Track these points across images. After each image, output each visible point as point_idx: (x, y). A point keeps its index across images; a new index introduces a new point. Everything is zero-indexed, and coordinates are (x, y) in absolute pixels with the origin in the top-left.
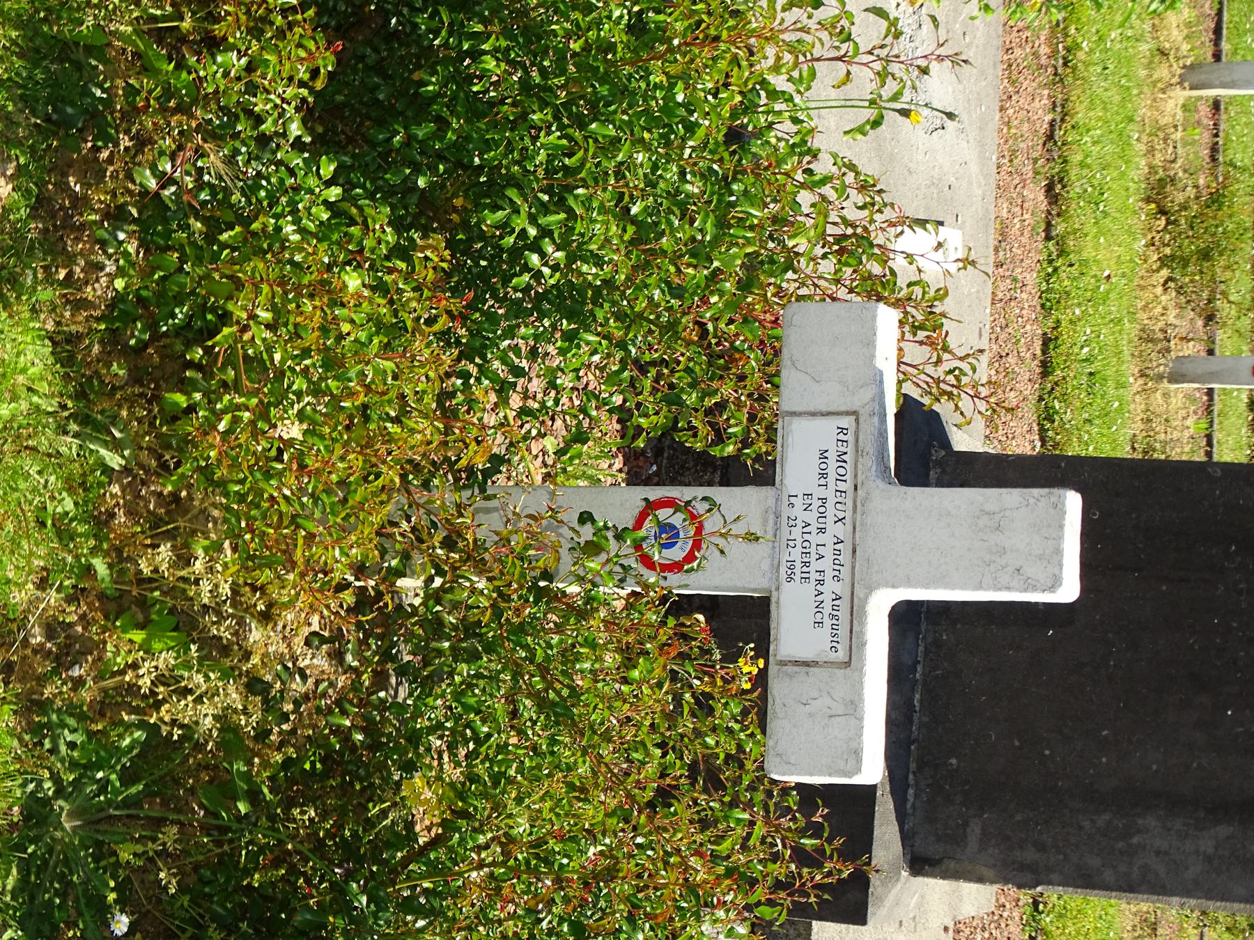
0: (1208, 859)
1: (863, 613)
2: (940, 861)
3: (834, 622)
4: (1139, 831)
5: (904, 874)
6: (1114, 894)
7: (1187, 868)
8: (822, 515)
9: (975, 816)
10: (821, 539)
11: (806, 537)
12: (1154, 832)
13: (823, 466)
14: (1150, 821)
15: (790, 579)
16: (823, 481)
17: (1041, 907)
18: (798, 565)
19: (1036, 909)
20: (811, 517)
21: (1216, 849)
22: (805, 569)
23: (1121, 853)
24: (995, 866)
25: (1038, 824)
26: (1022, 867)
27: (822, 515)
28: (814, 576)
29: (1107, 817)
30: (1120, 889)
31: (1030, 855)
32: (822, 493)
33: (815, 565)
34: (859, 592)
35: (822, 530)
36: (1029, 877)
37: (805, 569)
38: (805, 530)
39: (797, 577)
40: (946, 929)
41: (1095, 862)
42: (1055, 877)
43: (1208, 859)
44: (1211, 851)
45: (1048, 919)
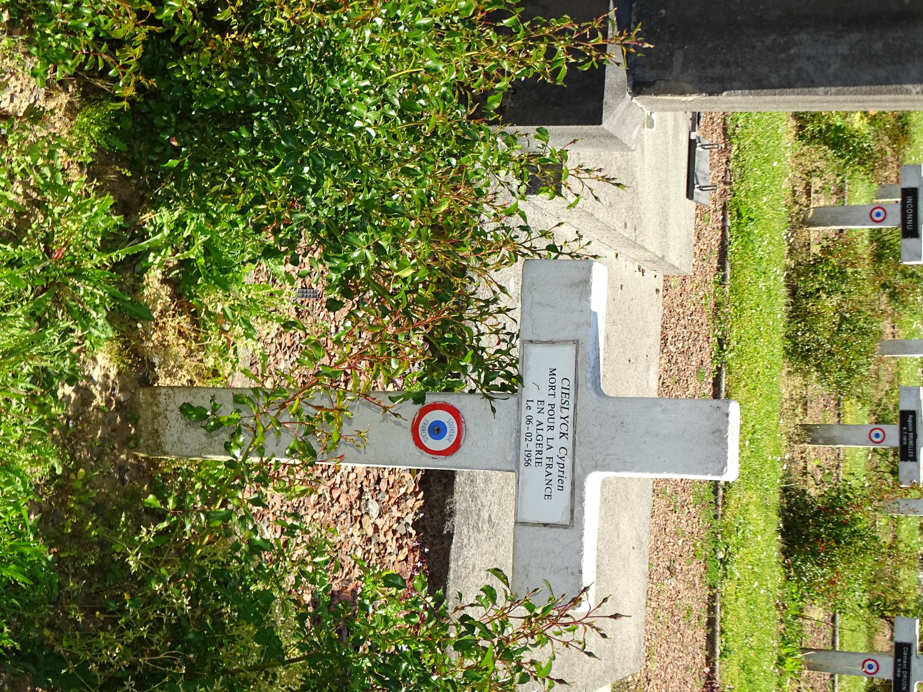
0: (844, 58)
1: (582, 488)
2: (654, 82)
3: (561, 474)
4: (796, 45)
5: (628, 96)
6: (777, 91)
7: (829, 66)
8: (551, 417)
9: (679, 48)
10: (550, 434)
11: (540, 432)
12: (805, 43)
13: (552, 381)
14: (804, 37)
15: (528, 464)
16: (552, 392)
17: (725, 347)
18: (534, 453)
19: (721, 348)
20: (543, 418)
21: (850, 50)
22: (538, 456)
23: (783, 61)
24: (692, 81)
25: (723, 49)
26: (712, 80)
27: (551, 417)
28: (545, 461)
29: (772, 37)
30: (782, 86)
31: (718, 71)
32: (551, 400)
33: (546, 453)
34: (578, 469)
35: (551, 428)
36: (717, 86)
37: (538, 456)
38: (539, 427)
39: (533, 463)
40: (657, 291)
41: (763, 70)
42: (735, 84)
43: (844, 58)
44: (846, 52)
45: (730, 356)
